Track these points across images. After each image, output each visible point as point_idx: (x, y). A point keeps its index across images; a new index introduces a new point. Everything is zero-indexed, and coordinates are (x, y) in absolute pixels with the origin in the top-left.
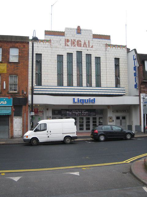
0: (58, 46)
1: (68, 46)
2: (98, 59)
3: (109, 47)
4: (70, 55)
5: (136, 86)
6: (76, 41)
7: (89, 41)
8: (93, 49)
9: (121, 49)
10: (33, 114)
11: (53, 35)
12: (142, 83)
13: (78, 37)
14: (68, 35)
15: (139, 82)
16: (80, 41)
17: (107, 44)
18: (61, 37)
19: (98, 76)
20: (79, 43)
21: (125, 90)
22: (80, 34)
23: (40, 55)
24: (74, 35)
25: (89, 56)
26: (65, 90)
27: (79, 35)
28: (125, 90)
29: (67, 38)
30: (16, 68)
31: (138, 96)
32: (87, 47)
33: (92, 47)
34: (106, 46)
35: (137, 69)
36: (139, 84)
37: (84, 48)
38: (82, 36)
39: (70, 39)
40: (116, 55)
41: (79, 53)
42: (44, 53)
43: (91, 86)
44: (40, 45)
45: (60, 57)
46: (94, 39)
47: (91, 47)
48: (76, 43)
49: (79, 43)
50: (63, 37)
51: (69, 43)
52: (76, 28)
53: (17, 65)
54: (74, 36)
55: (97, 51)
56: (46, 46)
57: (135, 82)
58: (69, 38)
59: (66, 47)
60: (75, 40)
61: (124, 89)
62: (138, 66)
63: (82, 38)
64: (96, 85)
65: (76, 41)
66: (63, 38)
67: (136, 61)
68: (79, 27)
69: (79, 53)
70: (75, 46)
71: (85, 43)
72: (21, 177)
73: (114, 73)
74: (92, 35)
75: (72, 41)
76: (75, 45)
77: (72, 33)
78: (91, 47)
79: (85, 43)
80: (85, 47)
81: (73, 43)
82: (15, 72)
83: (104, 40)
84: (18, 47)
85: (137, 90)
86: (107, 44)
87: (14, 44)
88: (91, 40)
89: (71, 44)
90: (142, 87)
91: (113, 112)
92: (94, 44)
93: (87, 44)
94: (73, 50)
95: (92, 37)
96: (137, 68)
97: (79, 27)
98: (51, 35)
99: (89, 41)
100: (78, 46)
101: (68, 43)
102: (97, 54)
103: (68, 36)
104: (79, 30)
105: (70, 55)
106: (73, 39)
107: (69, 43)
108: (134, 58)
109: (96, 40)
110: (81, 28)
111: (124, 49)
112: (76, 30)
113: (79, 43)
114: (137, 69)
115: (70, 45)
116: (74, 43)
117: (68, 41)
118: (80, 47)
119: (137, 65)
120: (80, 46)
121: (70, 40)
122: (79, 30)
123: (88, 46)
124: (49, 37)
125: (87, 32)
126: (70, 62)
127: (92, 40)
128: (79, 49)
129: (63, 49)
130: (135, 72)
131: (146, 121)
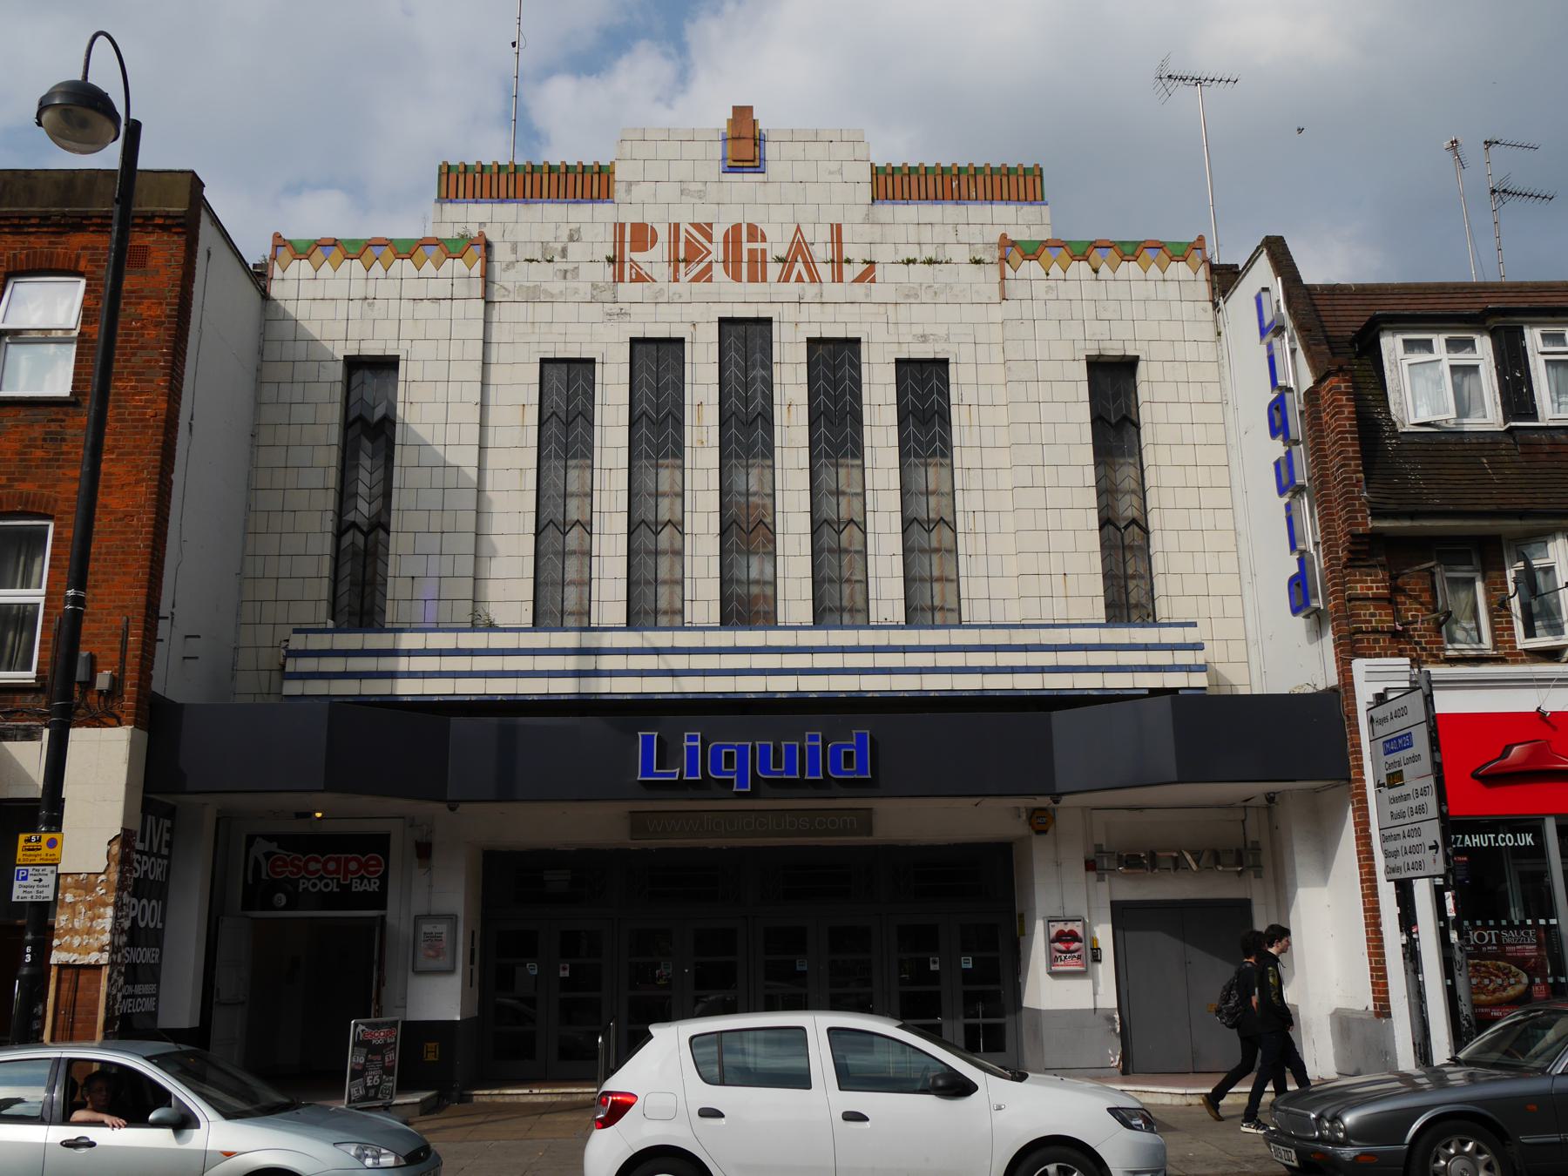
0: (557, 286)
1: (639, 278)
3: (1032, 268)
4: (657, 358)
5: (1299, 587)
6: (718, 233)
7: (837, 230)
8: (878, 291)
9: (1154, 271)
10: (281, 899)
11: (507, 199)
12: (1361, 551)
13: (736, 201)
14: (639, 192)
15: (1328, 543)
17: (1014, 244)
18: (581, 213)
20: (746, 246)
21: (1197, 647)
25: (834, 361)
27: (745, 183)
28: (1197, 647)
29: (630, 216)
30: (39, 453)
34: (1004, 259)
35: (1296, 427)
36: (1330, 568)
37: (792, 289)
41: (745, 339)
42: (421, 350)
43: (858, 615)
44: (386, 288)
45: (567, 381)
46: (885, 211)
47: (860, 279)
48: (717, 251)
49: (743, 252)
50: (604, 212)
51: (654, 259)
53: (54, 427)
54: (701, 195)
56: (439, 288)
57: (1293, 547)
58: (651, 216)
59: (628, 290)
60: (705, 229)
61: (1190, 635)
62: (1307, 381)
63: (772, 207)
64: (1412, 886)
65: (718, 233)
66: (593, 224)
67: (1284, 345)
68: (742, 114)
69: (745, 339)
70: (705, 275)
73: (1091, 498)
75: (683, 235)
76: (709, 267)
77: (682, 170)
78: (860, 279)
80: (800, 279)
82: (27, 487)
83: (978, 212)
84: (82, 266)
85: (1317, 632)
86: (1012, 237)
87: (40, 243)
88: (859, 213)
90: (1359, 589)
91: (1090, 866)
93: (822, 252)
94: (692, 314)
95: (866, 192)
96: (1295, 405)
97: (742, 114)
99: (837, 230)
100: (737, 277)
101: (637, 256)
102: (918, 330)
105: (657, 358)
106: (685, 217)
107: (654, 259)
108: (1261, 320)
109: (907, 212)
111: (1180, 269)
114: (1296, 427)
115: (662, 271)
116: (694, 253)
117: (642, 236)
118: (752, 279)
119: (1300, 375)
123: (825, 271)
124: (471, 217)
126: (657, 428)
127: (869, 220)
128: (743, 300)
130: (1278, 448)
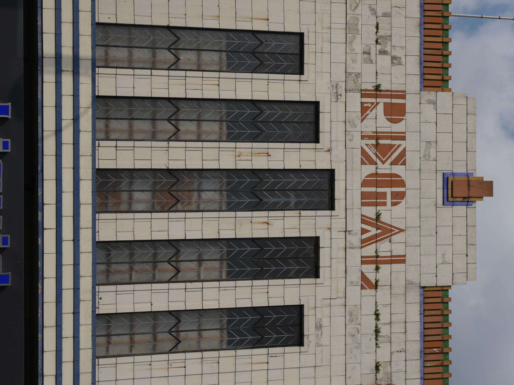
0: (358, 47)
1: (364, 109)
2: (283, 327)
4: (303, 122)
7: (401, 260)
8: (355, 292)
13: (423, 185)
14: (429, 110)
16: (398, 197)
18: (413, 65)
19: (171, 331)
20: (388, 191)
22: (445, 289)
23: (298, 71)
24: (433, 151)
25: (301, 258)
26: (68, 281)
27: (435, 189)
29: (411, 103)
32: (364, 243)
33: (367, 283)
37: (356, 225)
39: (409, 123)
40: (312, 35)
41: (317, 190)
45: (285, 52)
46: (415, 296)
48: (385, 168)
49: (382, 188)
50: (413, 84)
51: (379, 121)
52: (483, 171)
54: (427, 157)
55: (339, 321)
58: (411, 119)
59: (355, 101)
63: (419, 208)
65: (398, 169)
66: (405, 76)
68: (486, 188)
69: (317, 190)
70: (366, 160)
71: (387, 231)
74: (441, 283)
75: (397, 142)
80: (364, 231)
88: (413, 276)
93: (384, 248)
94: (337, 149)
95: (429, 281)
97: (486, 188)
98: (425, 353)
99: (401, 260)
100: (364, 184)
101: (380, 108)
103: (424, 117)
104: (464, 190)
106: (410, 144)
107: (379, 121)
109: (414, 314)
110: (482, 205)
112: (462, 170)
113: (382, 188)
116: (383, 151)
117: (396, 112)
118: (364, 195)
120: (367, 199)
121: (397, 128)
122: (464, 190)
126: (250, 121)
127: (408, 284)
128: (348, 187)
129: (339, 75)
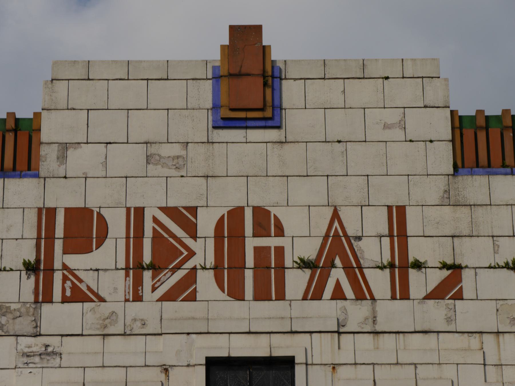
1: (77, 296)
7: (398, 216)
13: (239, 170)
14: (79, 160)
16: (265, 222)
20: (251, 243)
27: (247, 146)
29: (64, 197)
31: (416, 367)
33: (450, 287)
38: (292, 157)
39: (108, 201)
46: (475, 186)
47: (437, 294)
48: (204, 251)
51: (103, 265)
52: (210, 46)
54: (179, 163)
58: (98, 197)
59: (58, 315)
60: (185, 217)
63: (290, 182)
65: (206, 223)
68: (245, 39)
70: (184, 291)
71: (338, 245)
72: (336, 220)
74: (444, 129)
75: (149, 226)
78: (437, 294)
79: (338, 245)
80: (338, 294)
81: (158, 256)
88: (432, 189)
89: (135, 268)
92: (473, 253)
93: (373, 251)
95: (442, 157)
97: (245, 39)
99: (398, 216)
100: (236, 293)
101: (74, 261)
104: (248, 84)
106: (152, 197)
107: (103, 265)
112: (208, 85)
115: (114, 284)
116: (168, 252)
117: (84, 229)
118: (262, 295)
120: (269, 286)
121: (117, 225)
122: (248, 84)
123: (379, 282)
125: (363, 92)
127: (449, 200)
131: (270, 257)
